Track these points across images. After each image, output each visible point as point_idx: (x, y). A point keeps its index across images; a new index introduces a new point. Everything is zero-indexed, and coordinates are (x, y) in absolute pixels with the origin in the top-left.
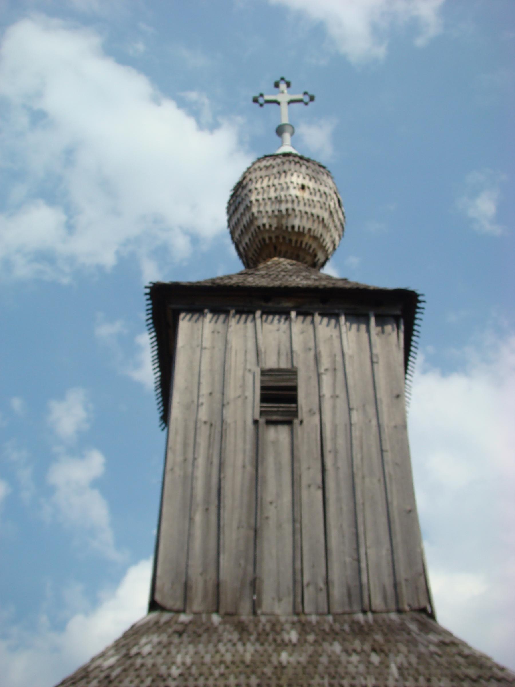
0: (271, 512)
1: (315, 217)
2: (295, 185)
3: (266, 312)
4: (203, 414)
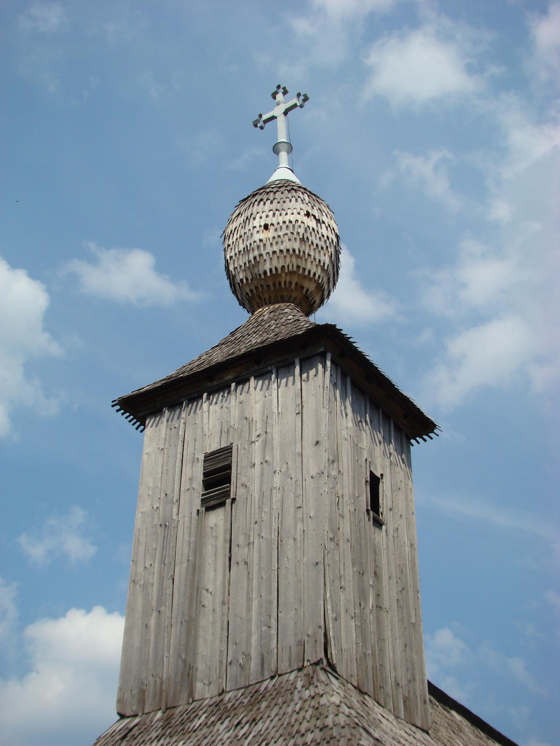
0: (207, 599)
1: (285, 253)
2: (258, 229)
3: (211, 393)
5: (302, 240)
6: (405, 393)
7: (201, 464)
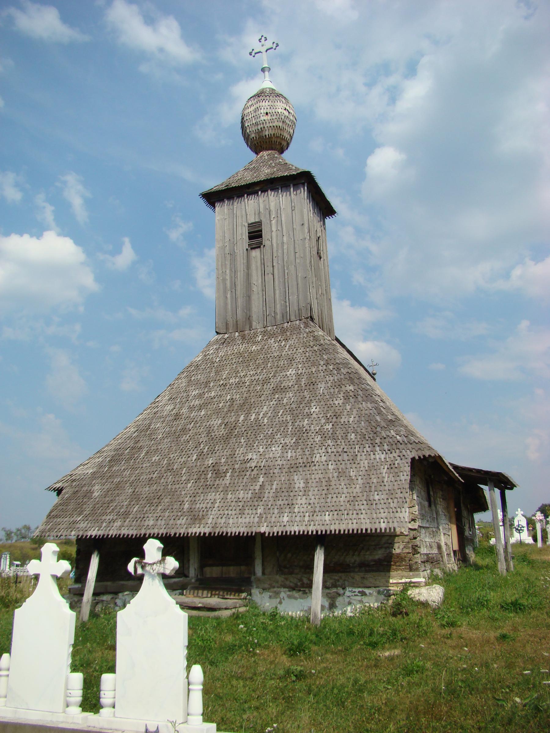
0: (255, 289)
4: (227, 251)
5: (283, 122)
6: (329, 200)
7: (247, 228)
